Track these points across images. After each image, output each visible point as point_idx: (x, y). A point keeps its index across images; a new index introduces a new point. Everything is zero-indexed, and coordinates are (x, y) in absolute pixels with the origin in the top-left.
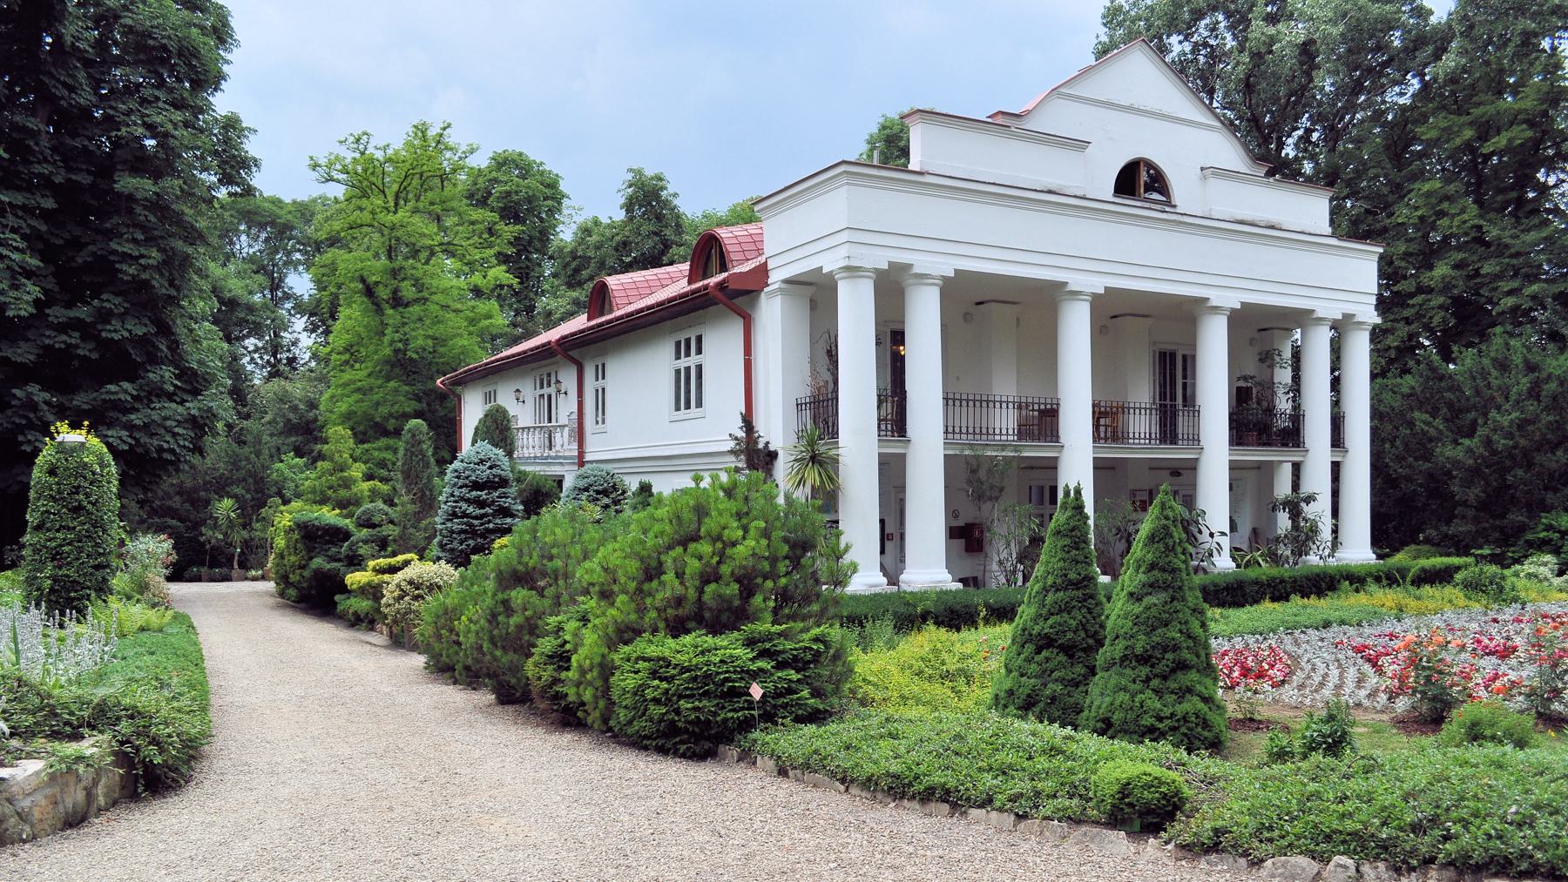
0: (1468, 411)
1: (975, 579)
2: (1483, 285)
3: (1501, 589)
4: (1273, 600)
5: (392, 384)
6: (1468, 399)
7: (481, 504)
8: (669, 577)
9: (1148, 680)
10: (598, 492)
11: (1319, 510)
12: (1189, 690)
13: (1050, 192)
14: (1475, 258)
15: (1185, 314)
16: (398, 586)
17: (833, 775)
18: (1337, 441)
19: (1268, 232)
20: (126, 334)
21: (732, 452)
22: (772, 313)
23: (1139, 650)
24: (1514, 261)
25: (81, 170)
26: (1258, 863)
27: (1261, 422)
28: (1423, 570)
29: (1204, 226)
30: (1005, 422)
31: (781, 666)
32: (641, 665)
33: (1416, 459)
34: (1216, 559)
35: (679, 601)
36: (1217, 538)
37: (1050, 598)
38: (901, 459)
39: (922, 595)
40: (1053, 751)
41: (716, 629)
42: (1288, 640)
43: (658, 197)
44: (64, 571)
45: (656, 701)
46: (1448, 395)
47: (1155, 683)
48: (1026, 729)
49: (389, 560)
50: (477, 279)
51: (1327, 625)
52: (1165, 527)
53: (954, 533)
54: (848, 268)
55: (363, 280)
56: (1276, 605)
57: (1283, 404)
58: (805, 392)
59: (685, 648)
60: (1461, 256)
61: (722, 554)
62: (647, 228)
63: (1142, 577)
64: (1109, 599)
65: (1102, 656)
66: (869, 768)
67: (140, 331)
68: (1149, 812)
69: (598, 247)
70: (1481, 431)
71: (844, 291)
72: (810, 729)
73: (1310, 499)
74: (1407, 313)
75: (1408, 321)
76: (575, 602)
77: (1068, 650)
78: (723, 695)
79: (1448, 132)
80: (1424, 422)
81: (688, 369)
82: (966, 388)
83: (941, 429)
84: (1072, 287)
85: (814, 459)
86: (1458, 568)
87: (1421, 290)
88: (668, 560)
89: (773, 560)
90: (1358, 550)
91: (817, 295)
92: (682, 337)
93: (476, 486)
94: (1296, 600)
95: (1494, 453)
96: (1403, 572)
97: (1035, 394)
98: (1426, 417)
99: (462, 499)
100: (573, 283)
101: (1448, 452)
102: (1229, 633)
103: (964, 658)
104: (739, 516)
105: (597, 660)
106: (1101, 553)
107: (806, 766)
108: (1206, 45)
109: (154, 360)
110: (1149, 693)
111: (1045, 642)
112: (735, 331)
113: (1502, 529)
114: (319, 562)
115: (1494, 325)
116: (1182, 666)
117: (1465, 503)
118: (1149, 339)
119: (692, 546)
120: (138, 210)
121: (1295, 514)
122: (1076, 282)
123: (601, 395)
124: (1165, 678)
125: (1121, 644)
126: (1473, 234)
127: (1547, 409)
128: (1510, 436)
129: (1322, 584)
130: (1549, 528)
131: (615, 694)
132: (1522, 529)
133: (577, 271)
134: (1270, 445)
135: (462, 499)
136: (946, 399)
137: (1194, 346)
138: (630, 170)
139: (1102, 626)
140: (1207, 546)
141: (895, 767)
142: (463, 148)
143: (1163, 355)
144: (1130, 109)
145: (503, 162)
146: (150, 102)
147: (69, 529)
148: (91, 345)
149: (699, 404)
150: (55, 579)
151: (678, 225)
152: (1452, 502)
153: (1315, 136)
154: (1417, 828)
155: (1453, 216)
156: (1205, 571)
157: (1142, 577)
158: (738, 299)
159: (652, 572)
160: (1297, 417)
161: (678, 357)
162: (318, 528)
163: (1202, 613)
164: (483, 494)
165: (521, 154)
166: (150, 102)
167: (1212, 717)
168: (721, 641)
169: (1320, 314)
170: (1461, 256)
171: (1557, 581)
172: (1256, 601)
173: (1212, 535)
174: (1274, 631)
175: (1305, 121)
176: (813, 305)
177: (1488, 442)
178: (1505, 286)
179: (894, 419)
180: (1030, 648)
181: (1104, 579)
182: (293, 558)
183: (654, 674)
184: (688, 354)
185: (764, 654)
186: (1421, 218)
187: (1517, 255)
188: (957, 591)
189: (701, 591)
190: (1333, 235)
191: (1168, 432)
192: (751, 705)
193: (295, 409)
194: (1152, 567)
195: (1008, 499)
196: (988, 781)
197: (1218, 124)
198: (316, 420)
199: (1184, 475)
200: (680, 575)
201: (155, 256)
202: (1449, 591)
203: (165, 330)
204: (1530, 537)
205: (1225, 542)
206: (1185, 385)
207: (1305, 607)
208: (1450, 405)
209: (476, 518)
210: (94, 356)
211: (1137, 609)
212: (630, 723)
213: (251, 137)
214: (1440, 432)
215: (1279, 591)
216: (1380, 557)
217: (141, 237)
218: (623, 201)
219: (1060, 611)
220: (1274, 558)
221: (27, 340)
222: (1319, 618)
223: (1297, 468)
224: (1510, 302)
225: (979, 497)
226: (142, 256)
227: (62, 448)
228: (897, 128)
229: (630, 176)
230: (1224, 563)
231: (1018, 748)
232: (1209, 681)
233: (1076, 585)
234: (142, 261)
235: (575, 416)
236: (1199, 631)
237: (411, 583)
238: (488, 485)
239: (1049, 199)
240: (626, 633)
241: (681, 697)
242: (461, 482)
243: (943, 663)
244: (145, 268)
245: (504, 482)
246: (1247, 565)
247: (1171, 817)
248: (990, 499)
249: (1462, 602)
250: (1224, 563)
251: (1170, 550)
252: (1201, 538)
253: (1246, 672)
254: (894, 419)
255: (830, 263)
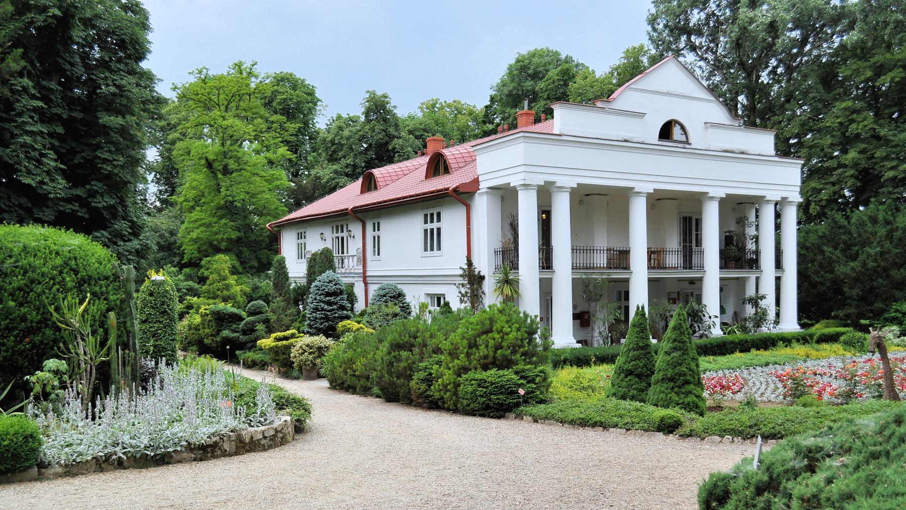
0: (855, 245)
1: (586, 341)
2: (876, 163)
3: (863, 345)
4: (741, 351)
5: (223, 221)
6: (855, 239)
7: (329, 303)
8: (482, 347)
9: (673, 388)
10: (391, 297)
11: (769, 303)
12: (690, 392)
13: (626, 141)
14: (871, 147)
15: (697, 200)
16: (301, 347)
17: (557, 421)
18: (779, 265)
19: (741, 155)
20: (105, 204)
21: (461, 276)
22: (482, 204)
23: (669, 376)
24: (894, 150)
25: (76, 110)
26: (703, 439)
27: (737, 255)
28: (824, 335)
29: (706, 154)
30: (601, 260)
31: (528, 382)
32: (473, 382)
33: (826, 272)
34: (712, 330)
35: (486, 357)
36: (713, 319)
37: (631, 354)
38: (550, 281)
39: (563, 351)
40: (637, 410)
41: (501, 367)
42: (746, 372)
43: (384, 108)
44: (159, 343)
45: (481, 396)
46: (843, 237)
47: (676, 389)
48: (626, 404)
49: (283, 333)
50: (270, 155)
51: (767, 364)
52: (680, 324)
53: (576, 316)
54: (524, 185)
55: (207, 159)
56: (742, 354)
57: (751, 246)
58: (498, 246)
59: (491, 374)
60: (863, 146)
61: (502, 338)
62: (378, 128)
63: (670, 345)
64: (656, 353)
65: (653, 379)
66: (571, 417)
67: (112, 202)
68: (670, 426)
69: (348, 139)
70: (861, 257)
71: (522, 196)
72: (542, 406)
73: (763, 297)
74: (832, 179)
75: (834, 184)
76: (431, 357)
77: (639, 376)
78: (508, 393)
79: (857, 72)
80: (831, 253)
81: (432, 230)
82: (581, 244)
83: (571, 265)
84: (636, 190)
85: (507, 281)
86: (843, 334)
87: (841, 166)
88: (480, 341)
89: (522, 340)
90: (790, 324)
91: (506, 196)
92: (429, 212)
93: (328, 294)
94: (754, 351)
95: (867, 269)
96: (812, 336)
97: (619, 246)
98: (830, 249)
99: (321, 301)
100: (332, 159)
101: (845, 269)
102: (712, 369)
103: (590, 380)
104: (507, 322)
105: (452, 380)
106: (652, 327)
107: (546, 418)
108: (714, 14)
109: (114, 216)
110: (673, 394)
111: (629, 373)
112: (461, 212)
113: (872, 311)
114: (226, 333)
115: (882, 187)
116: (687, 382)
117: (850, 297)
118: (679, 214)
119: (490, 335)
120: (112, 134)
121: (756, 305)
122: (639, 187)
123: (377, 241)
124: (680, 387)
125: (661, 373)
126: (871, 133)
127: (896, 247)
128: (875, 260)
129: (768, 343)
130: (897, 311)
131: (461, 394)
132: (882, 311)
133: (334, 152)
134: (741, 268)
135: (321, 301)
136: (573, 249)
137: (701, 213)
138: (368, 92)
139: (654, 366)
140: (707, 323)
141: (581, 416)
142: (263, 75)
143: (685, 218)
144: (667, 94)
145: (281, 80)
146: (115, 72)
147: (160, 322)
148: (84, 210)
149: (439, 249)
150: (155, 346)
151: (396, 125)
152: (834, 299)
153: (780, 70)
154: (750, 427)
155: (859, 122)
156: (707, 337)
157: (670, 345)
158: (462, 196)
159: (473, 345)
160: (757, 252)
161: (426, 222)
162: (226, 314)
163: (697, 360)
164: (332, 299)
165: (291, 75)
166: (115, 72)
167: (700, 404)
168: (505, 372)
169: (768, 198)
170: (863, 146)
171: (897, 341)
172: (733, 353)
173: (710, 317)
174: (739, 368)
175: (773, 62)
176: (503, 199)
177: (864, 264)
178: (888, 164)
179: (546, 261)
180: (622, 375)
181: (654, 341)
182: (207, 331)
183: (479, 386)
184: (432, 222)
185: (522, 377)
186: (841, 123)
187: (896, 146)
188: (580, 348)
189: (495, 352)
190: (777, 155)
191: (688, 263)
192: (519, 397)
193: (161, 236)
194: (675, 340)
195: (604, 300)
196: (615, 419)
197: (713, 98)
198: (175, 242)
199: (697, 283)
200: (487, 346)
201: (122, 159)
202: (836, 347)
203: (122, 202)
204: (886, 316)
205: (718, 321)
206: (697, 235)
207: (757, 355)
208: (845, 242)
209: (329, 311)
210: (87, 216)
211: (669, 358)
212: (468, 405)
213: (160, 84)
214: (839, 258)
215: (744, 347)
216: (803, 326)
217: (113, 149)
218: (363, 110)
219: (636, 360)
220: (744, 329)
221: (48, 207)
222: (764, 361)
223: (757, 279)
224: (891, 174)
225: (590, 300)
226: (114, 160)
227: (154, 283)
228: (527, 62)
229: (367, 95)
230: (717, 332)
231: (625, 409)
232: (699, 389)
233: (642, 348)
234: (115, 163)
235: (361, 250)
236: (694, 368)
237: (308, 346)
238: (334, 294)
239: (625, 144)
240: (462, 370)
241: (491, 394)
242: (320, 292)
243: (581, 383)
244: (115, 166)
245: (341, 292)
246: (729, 333)
247: (677, 428)
248: (595, 300)
249: (841, 352)
250: (717, 332)
251: (682, 333)
252: (705, 319)
253: (723, 387)
254: (546, 261)
255: (515, 181)
